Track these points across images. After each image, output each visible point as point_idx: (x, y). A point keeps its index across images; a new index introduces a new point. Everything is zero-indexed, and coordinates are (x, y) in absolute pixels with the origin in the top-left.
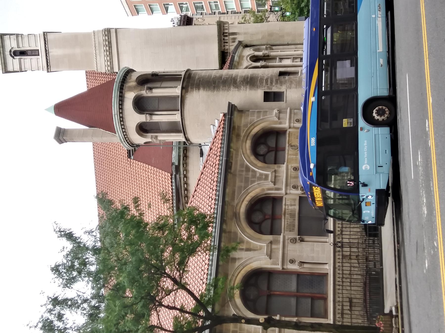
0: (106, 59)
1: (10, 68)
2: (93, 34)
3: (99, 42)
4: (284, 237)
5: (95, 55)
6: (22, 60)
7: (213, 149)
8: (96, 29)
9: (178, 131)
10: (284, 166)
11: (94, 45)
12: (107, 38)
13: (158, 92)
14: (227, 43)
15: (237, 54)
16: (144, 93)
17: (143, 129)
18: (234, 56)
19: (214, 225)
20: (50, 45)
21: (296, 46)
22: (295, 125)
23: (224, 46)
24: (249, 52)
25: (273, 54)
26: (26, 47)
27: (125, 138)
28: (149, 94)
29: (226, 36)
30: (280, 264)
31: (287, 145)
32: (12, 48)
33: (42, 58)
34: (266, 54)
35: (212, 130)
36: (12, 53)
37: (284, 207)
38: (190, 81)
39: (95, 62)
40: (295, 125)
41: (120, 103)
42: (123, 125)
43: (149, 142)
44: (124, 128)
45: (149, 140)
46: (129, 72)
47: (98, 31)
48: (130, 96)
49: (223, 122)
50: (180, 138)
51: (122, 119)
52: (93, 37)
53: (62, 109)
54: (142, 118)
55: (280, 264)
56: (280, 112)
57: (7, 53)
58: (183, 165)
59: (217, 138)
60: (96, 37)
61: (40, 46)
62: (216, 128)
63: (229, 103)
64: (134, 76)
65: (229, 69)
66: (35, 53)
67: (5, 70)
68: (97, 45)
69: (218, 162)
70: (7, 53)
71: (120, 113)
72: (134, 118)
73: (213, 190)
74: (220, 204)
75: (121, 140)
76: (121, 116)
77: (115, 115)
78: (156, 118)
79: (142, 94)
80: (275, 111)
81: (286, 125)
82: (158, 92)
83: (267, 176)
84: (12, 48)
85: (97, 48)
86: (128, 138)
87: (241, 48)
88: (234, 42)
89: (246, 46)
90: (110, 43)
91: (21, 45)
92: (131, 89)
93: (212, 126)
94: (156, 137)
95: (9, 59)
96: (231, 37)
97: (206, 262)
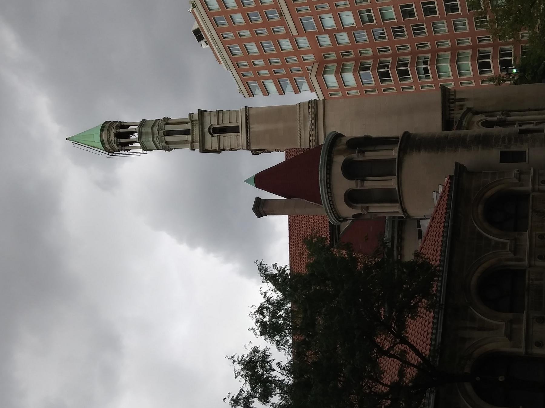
1: (208, 147)
2: (298, 107)
3: (304, 115)
4: (528, 316)
6: (221, 138)
9: (392, 201)
10: (527, 234)
11: (298, 118)
12: (313, 110)
13: (372, 155)
14: (453, 110)
15: (465, 119)
16: (356, 156)
17: (352, 198)
18: (462, 121)
19: (440, 279)
20: (251, 121)
21: (540, 111)
22: (540, 187)
23: (449, 114)
24: (478, 118)
25: (510, 118)
26: (227, 124)
27: (332, 208)
28: (361, 158)
29: (452, 103)
30: (523, 347)
31: (530, 210)
33: (242, 136)
34: (502, 119)
35: (435, 198)
37: (527, 281)
38: (409, 143)
40: (540, 187)
41: (328, 167)
42: (330, 192)
45: (360, 212)
46: (337, 137)
47: (304, 103)
48: (339, 160)
49: (448, 185)
50: (394, 209)
52: (298, 110)
53: (262, 180)
54: (351, 185)
55: (523, 347)
56: (521, 173)
57: (206, 130)
59: (441, 204)
60: (302, 109)
61: (241, 123)
62: (439, 195)
63: (457, 163)
64: (344, 141)
65: (457, 129)
66: (235, 129)
68: (302, 118)
69: (430, 330)
70: (206, 130)
71: (327, 179)
72: (343, 185)
73: (428, 334)
74: (440, 330)
75: (326, 210)
77: (321, 181)
78: (368, 185)
79: (353, 158)
80: (515, 172)
81: (529, 187)
82: (372, 155)
83: (505, 245)
84: (212, 125)
85: (302, 122)
86: (335, 209)
87: (470, 114)
88: (462, 109)
89: (477, 113)
90: (316, 116)
91: (221, 122)
92: (341, 153)
93: (434, 193)
94: (367, 208)
95: (208, 136)
96: (458, 103)
97: (427, 342)
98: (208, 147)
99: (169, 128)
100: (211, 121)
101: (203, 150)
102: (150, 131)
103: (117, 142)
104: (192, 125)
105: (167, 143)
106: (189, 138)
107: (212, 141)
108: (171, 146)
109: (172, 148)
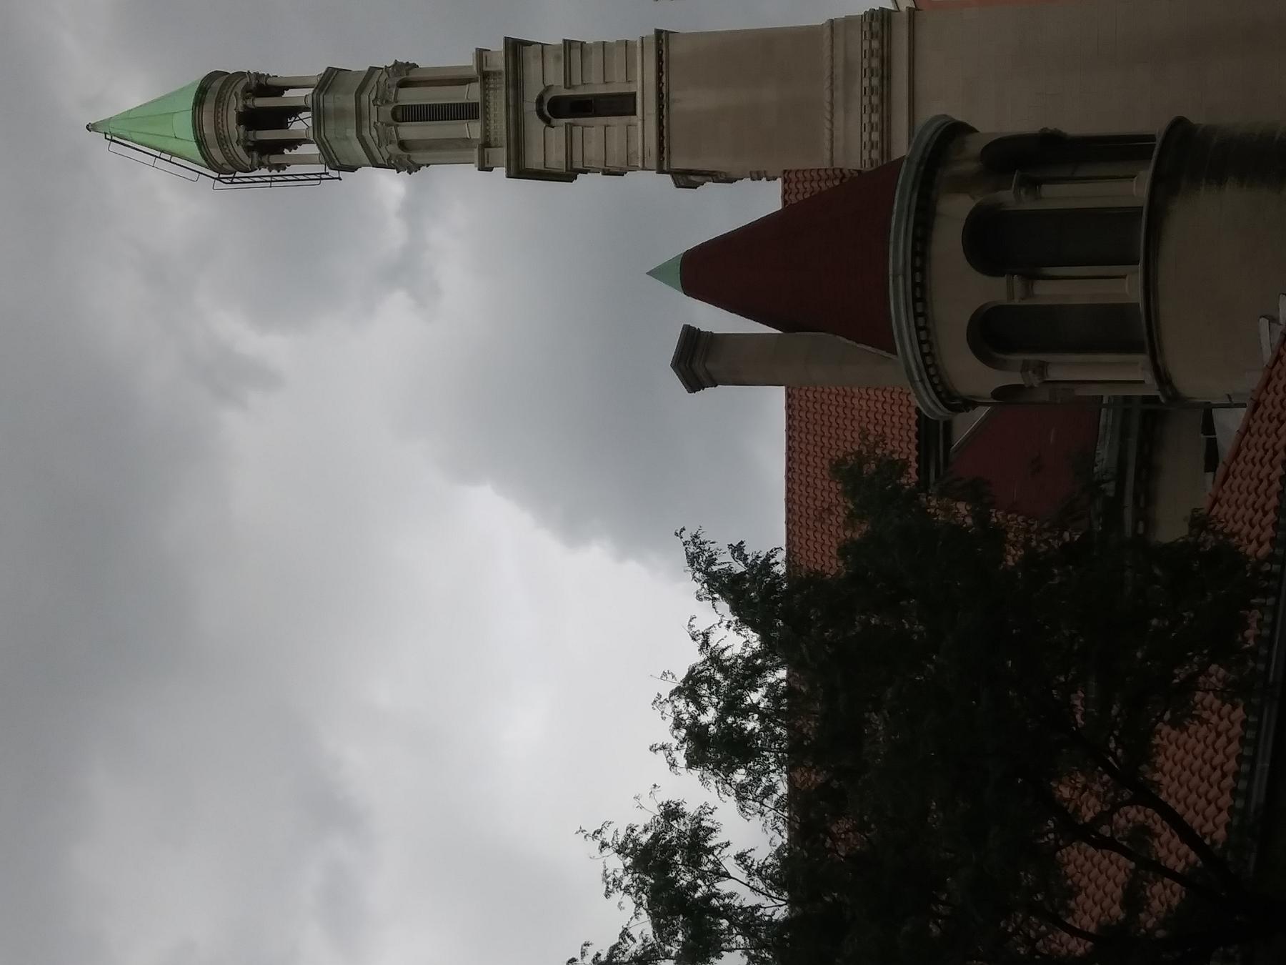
0: (866, 119)
1: (534, 160)
2: (828, 31)
5: (828, 107)
6: (577, 132)
7: (1268, 402)
8: (839, 13)
11: (827, 73)
13: (1061, 195)
16: (1010, 198)
17: (991, 335)
19: (1271, 601)
26: (595, 86)
28: (1028, 205)
32: (548, 89)
33: (641, 128)
36: (545, 108)
39: (827, 132)
43: (1018, 388)
44: (926, 342)
45: (1015, 378)
46: (953, 132)
47: (848, 20)
48: (955, 210)
51: (920, 295)
52: (827, 43)
53: (704, 271)
54: (994, 290)
57: (530, 106)
58: (1136, 499)
61: (642, 83)
64: (974, 146)
66: (622, 105)
67: (518, 166)
68: (839, 71)
69: (1232, 764)
70: (530, 106)
71: (914, 269)
72: (963, 290)
73: (1224, 776)
76: (919, 310)
77: (896, 276)
78: (1047, 292)
82: (1061, 195)
84: (548, 89)
91: (576, 80)
92: (961, 184)
93: (1264, 323)
94: (1042, 368)
95: (534, 125)
98: (534, 160)
99: (411, 97)
100: (544, 78)
101: (519, 171)
102: (350, 103)
103: (246, 140)
104: (485, 90)
105: (402, 145)
106: (474, 130)
107: (547, 142)
108: (417, 157)
109: (418, 161)
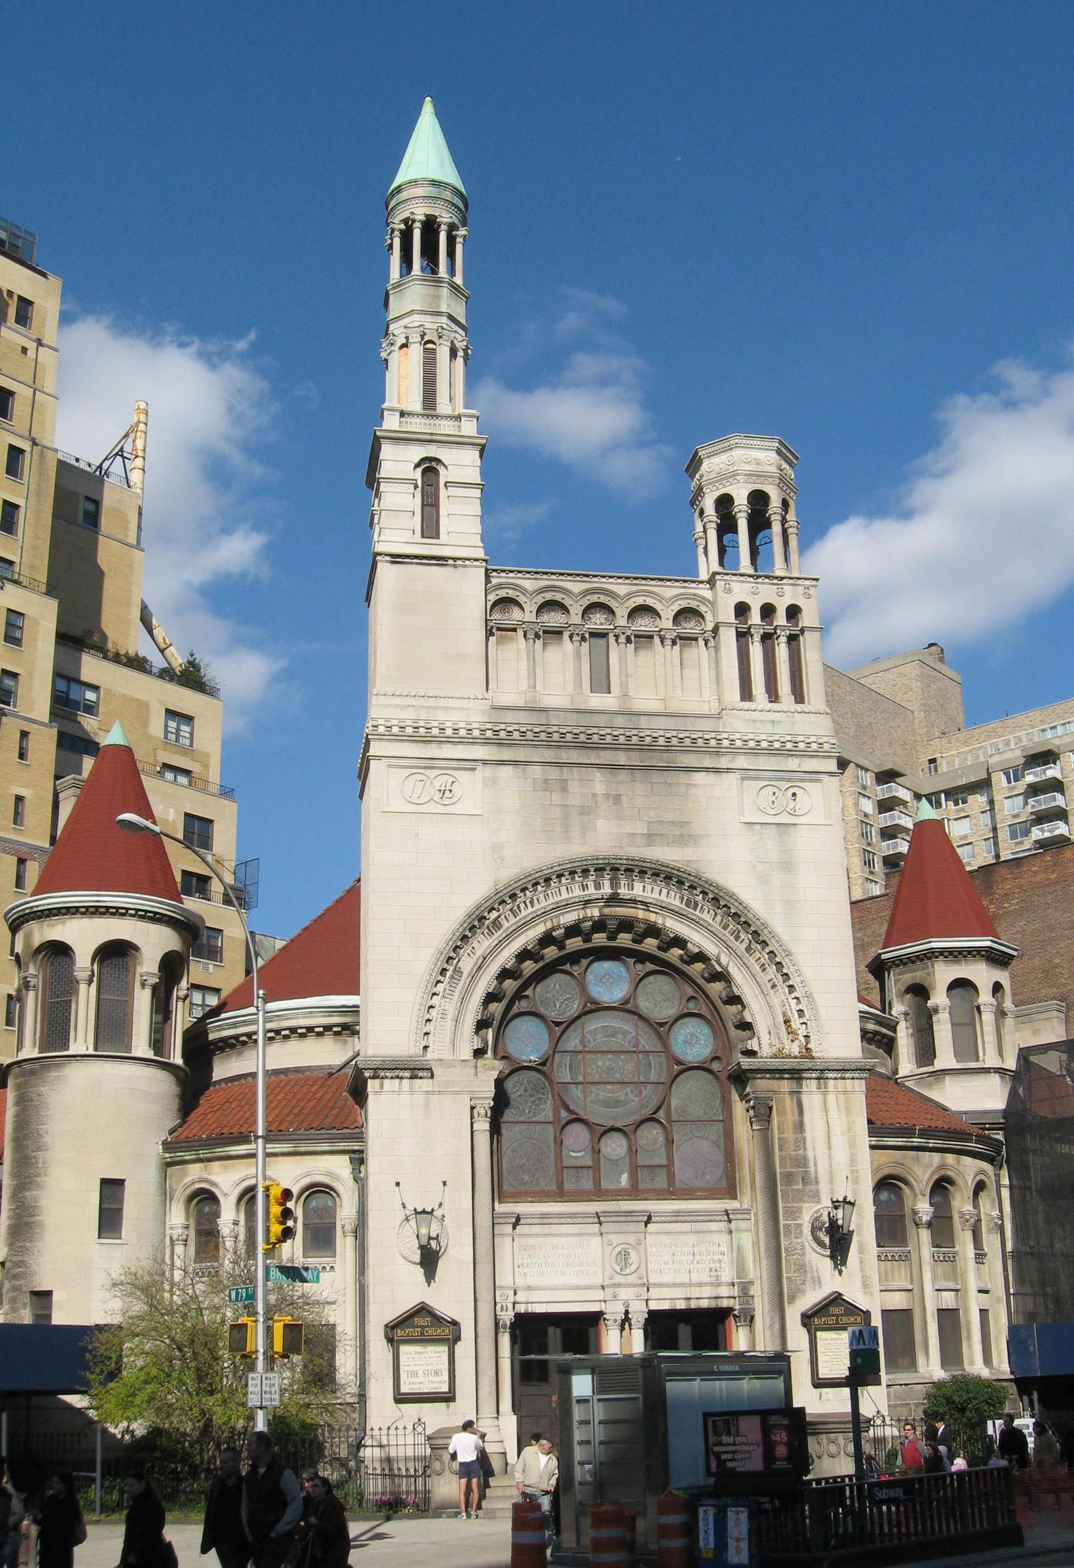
95: (418, 452)
102: (444, 308)
103: (414, 221)
